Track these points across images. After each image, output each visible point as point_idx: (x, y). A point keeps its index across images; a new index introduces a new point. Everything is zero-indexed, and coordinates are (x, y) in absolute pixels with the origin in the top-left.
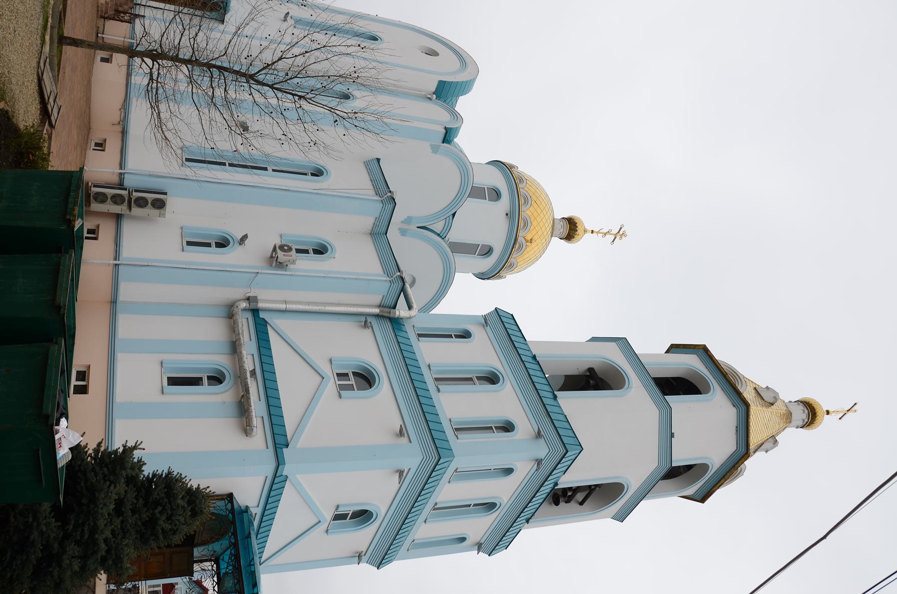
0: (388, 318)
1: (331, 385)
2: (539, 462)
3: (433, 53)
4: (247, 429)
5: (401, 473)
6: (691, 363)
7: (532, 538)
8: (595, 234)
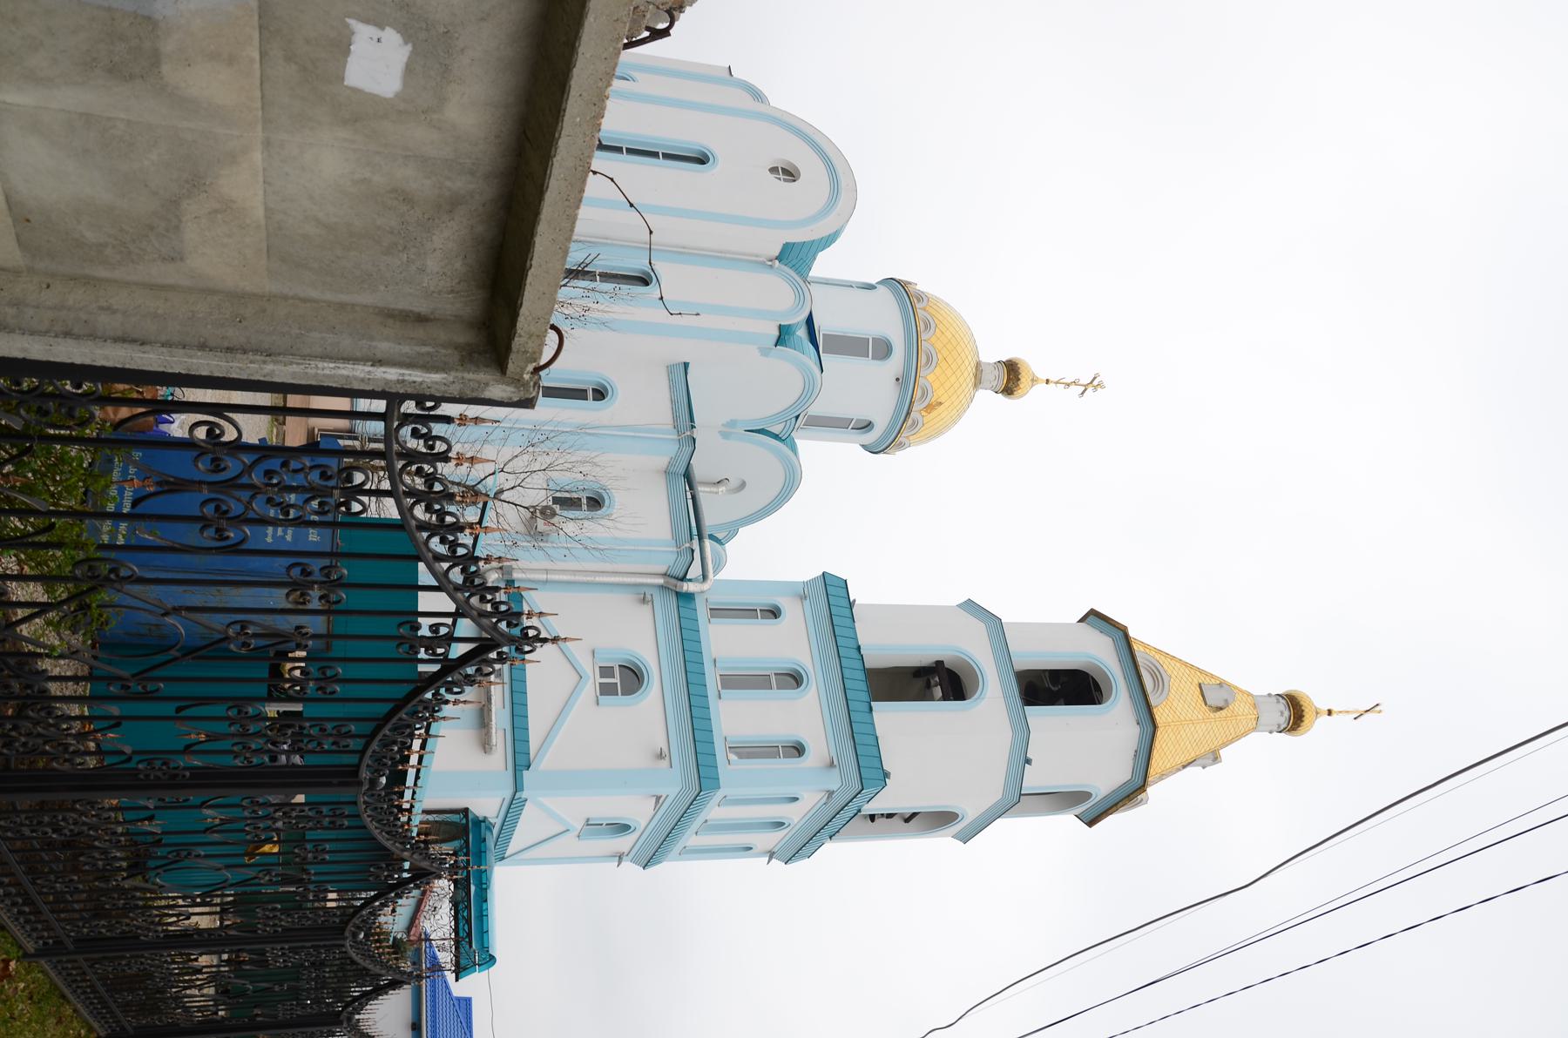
0: (677, 592)
1: (590, 688)
2: (831, 793)
3: (790, 174)
4: (486, 745)
5: (658, 798)
6: (1096, 653)
7: (831, 851)
8: (1051, 385)
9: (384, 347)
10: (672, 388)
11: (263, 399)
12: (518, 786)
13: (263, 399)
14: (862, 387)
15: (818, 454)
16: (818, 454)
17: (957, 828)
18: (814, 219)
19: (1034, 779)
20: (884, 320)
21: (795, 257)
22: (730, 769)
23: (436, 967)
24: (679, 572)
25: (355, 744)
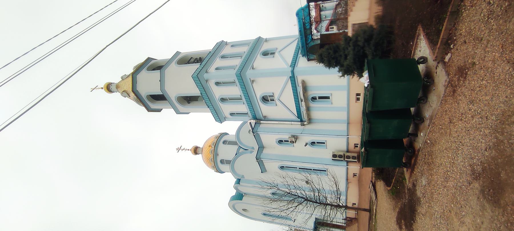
0: (258, 119)
2: (207, 72)
4: (303, 82)
6: (153, 106)
7: (208, 46)
20: (221, 167)
22: (234, 78)
24: (257, 125)
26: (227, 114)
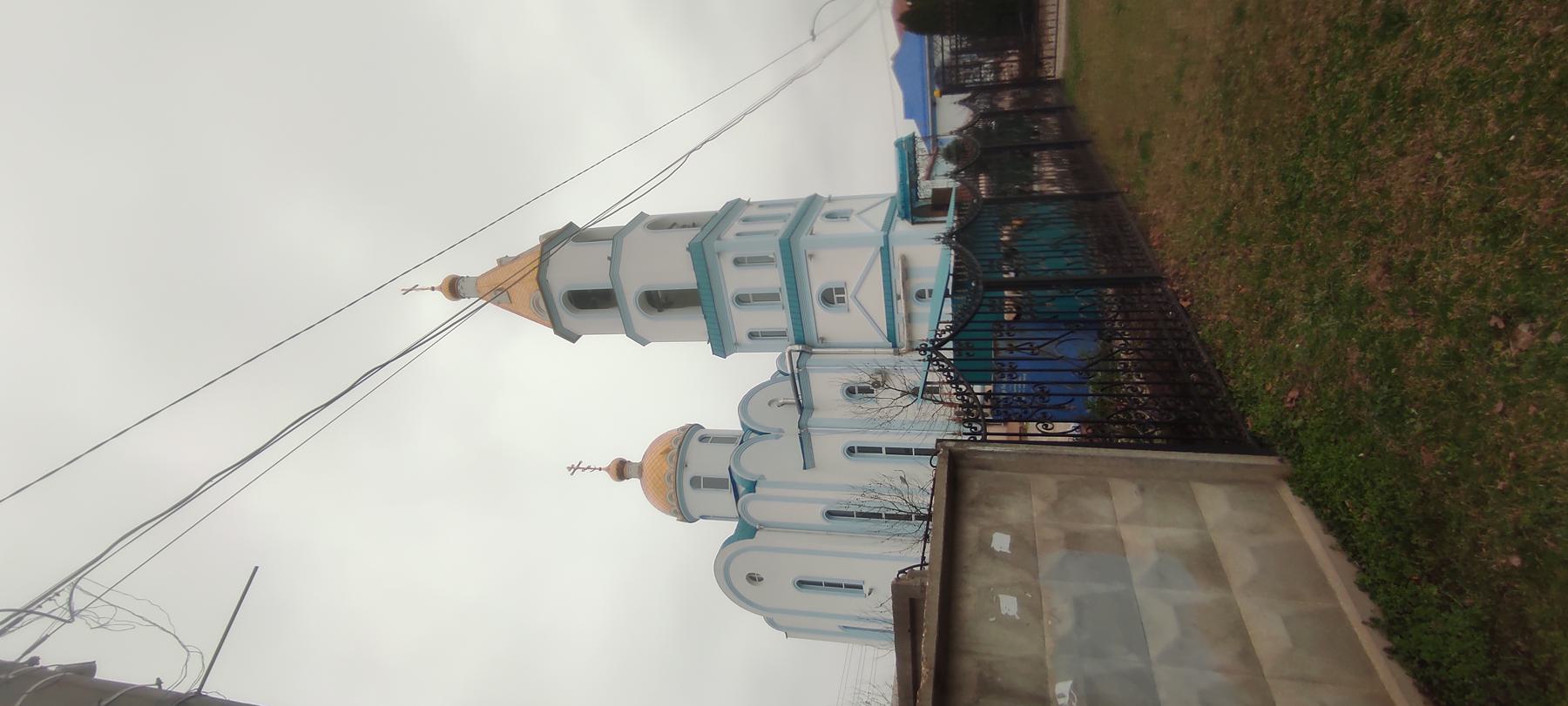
1: (850, 291)
3: (752, 578)
4: (904, 259)
6: (569, 319)
7: (716, 205)
9: (990, 458)
10: (812, 455)
11: (1031, 439)
12: (886, 238)
13: (1031, 439)
14: (711, 461)
15: (728, 421)
16: (728, 421)
17: (647, 220)
18: (738, 553)
19: (606, 249)
20: (696, 499)
21: (747, 530)
22: (774, 250)
23: (925, 139)
25: (986, 301)
26: (742, 335)
